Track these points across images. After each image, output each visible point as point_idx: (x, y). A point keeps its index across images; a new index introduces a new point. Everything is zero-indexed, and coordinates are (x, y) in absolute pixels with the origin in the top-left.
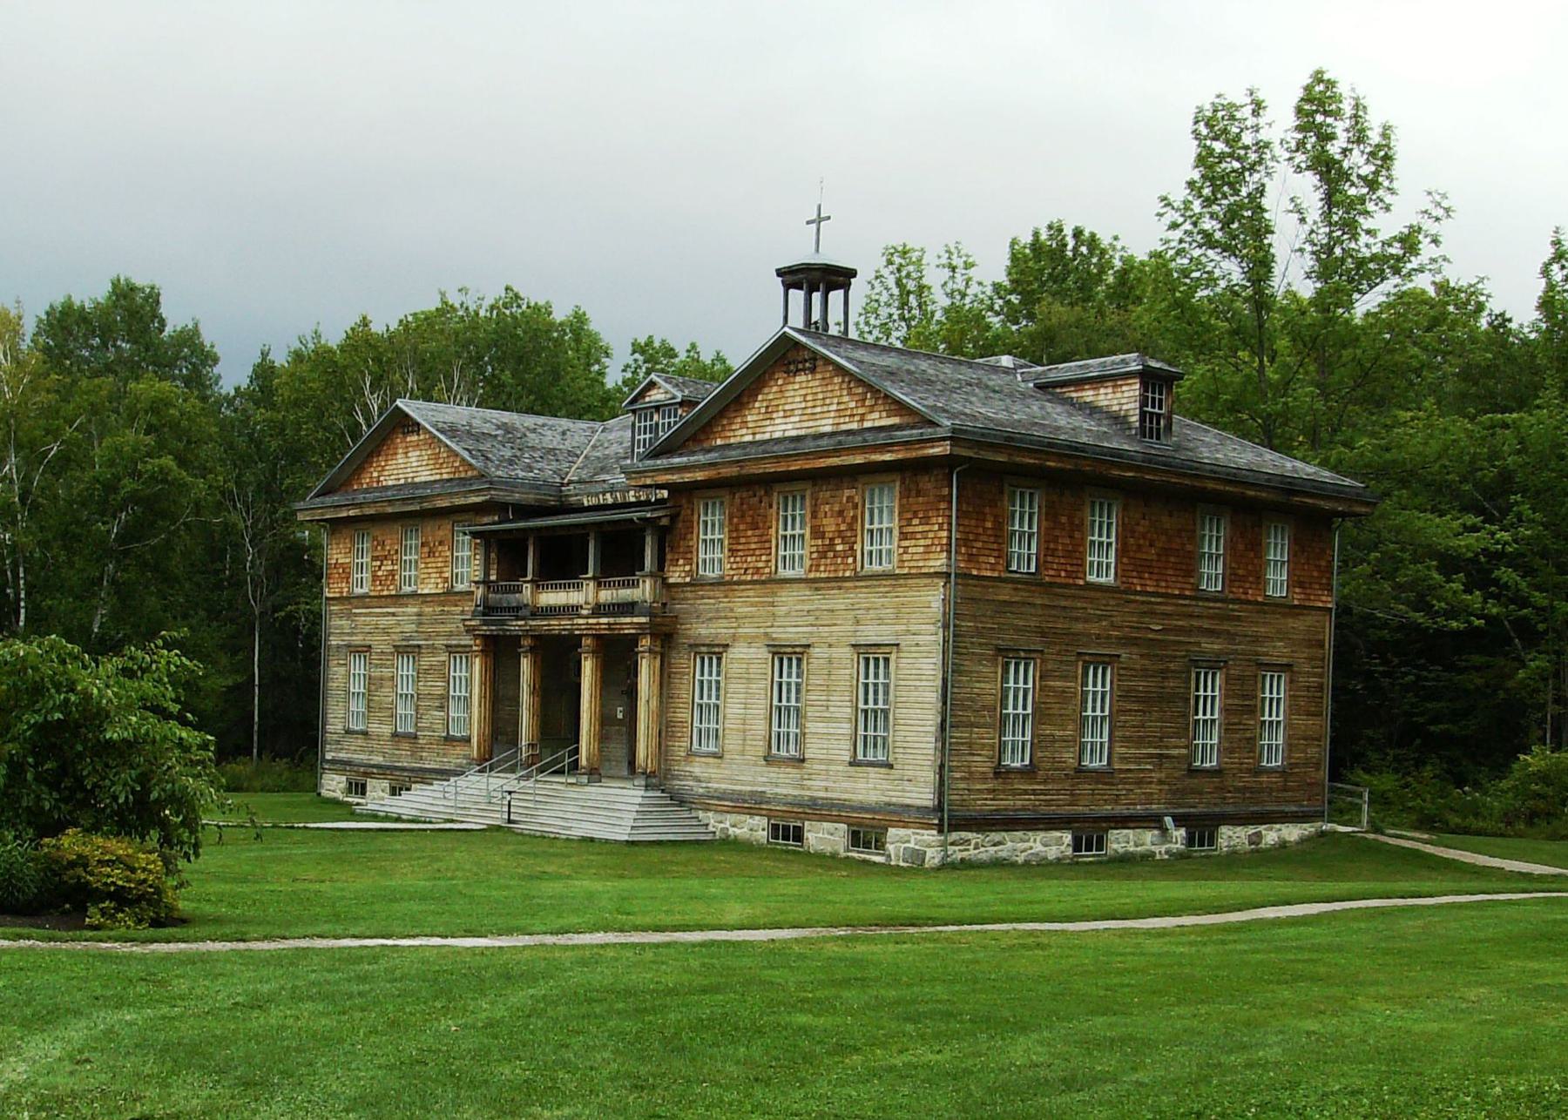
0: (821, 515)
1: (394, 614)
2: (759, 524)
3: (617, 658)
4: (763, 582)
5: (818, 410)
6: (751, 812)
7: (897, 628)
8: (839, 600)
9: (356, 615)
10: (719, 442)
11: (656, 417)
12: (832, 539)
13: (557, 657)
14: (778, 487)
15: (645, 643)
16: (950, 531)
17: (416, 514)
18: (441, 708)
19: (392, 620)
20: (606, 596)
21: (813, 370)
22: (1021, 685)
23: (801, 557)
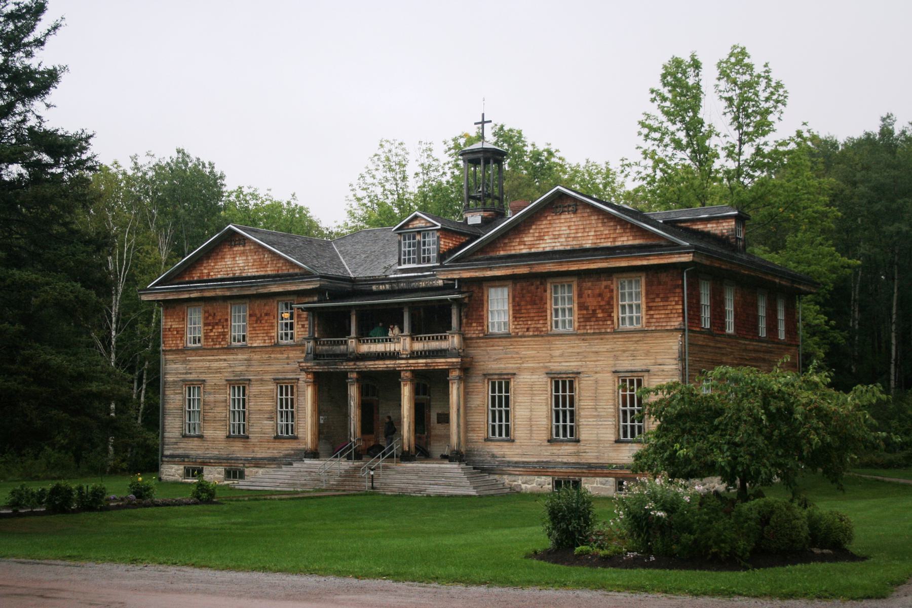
0: (585, 295)
1: (225, 360)
3: (430, 384)
4: (542, 336)
5: (580, 235)
6: (539, 473)
7: (647, 361)
8: (602, 346)
9: (190, 361)
10: (502, 253)
11: (418, 238)
12: (594, 311)
13: (378, 387)
14: (550, 281)
15: (455, 374)
16: (683, 305)
18: (271, 419)
20: (418, 346)
22: (284, 397)
23: (570, 321)
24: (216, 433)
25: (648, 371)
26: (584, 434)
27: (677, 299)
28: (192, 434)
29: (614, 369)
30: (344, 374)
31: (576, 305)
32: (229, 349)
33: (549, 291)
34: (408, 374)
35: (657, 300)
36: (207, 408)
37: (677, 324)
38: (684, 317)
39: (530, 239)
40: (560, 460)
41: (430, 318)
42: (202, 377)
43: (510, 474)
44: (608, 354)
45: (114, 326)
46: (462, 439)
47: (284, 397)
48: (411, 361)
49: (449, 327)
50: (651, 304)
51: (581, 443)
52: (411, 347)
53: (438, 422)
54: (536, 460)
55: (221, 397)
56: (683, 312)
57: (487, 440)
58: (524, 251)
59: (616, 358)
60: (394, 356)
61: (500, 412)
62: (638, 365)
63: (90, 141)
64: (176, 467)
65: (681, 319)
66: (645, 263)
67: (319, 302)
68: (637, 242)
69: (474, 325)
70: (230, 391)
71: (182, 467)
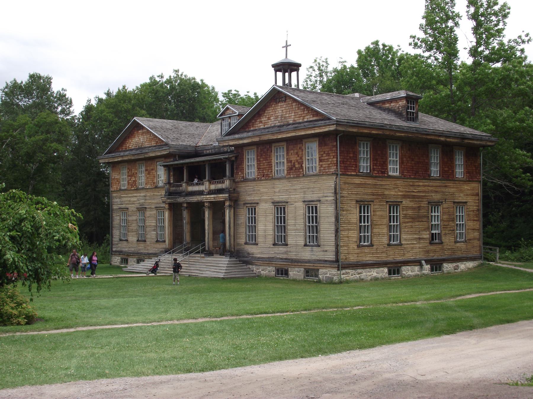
0: (290, 154)
1: (136, 196)
3: (217, 208)
5: (287, 115)
6: (269, 265)
9: (122, 197)
14: (274, 145)
15: (227, 204)
20: (213, 187)
21: (285, 101)
24: (133, 238)
25: (320, 201)
27: (333, 154)
29: (303, 200)
30: (181, 204)
31: (286, 160)
32: (137, 189)
33: (273, 151)
34: (185, 205)
35: (324, 155)
36: (129, 224)
37: (333, 170)
38: (337, 166)
39: (265, 119)
40: (278, 256)
41: (217, 170)
42: (128, 206)
43: (256, 265)
44: (301, 191)
46: (232, 242)
47: (311, 215)
48: (208, 196)
49: (225, 175)
51: (289, 246)
52: (209, 187)
54: (267, 256)
55: (134, 218)
56: (337, 163)
57: (246, 243)
58: (262, 127)
59: (305, 193)
60: (201, 193)
62: (315, 197)
64: (117, 258)
65: (335, 167)
66: (313, 132)
67: (174, 161)
68: (315, 118)
69: (240, 173)
70: (138, 214)
71: (120, 258)
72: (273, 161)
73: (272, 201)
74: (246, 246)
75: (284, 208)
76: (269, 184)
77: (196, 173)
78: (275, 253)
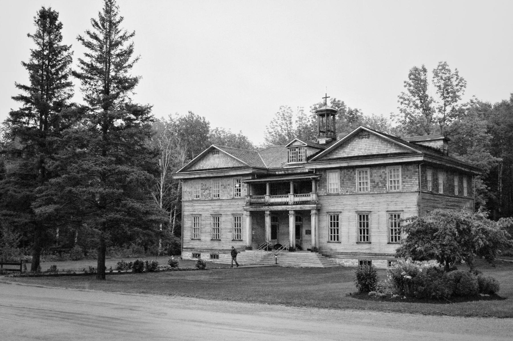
2: (351, 179)
3: (302, 217)
12: (378, 183)
13: (280, 218)
14: (357, 169)
17: (219, 175)
19: (209, 207)
20: (297, 199)
21: (368, 138)
25: (403, 211)
26: (373, 239)
28: (196, 238)
41: (303, 186)
42: (200, 213)
45: (162, 190)
50: (404, 180)
51: (372, 244)
53: (306, 234)
54: (351, 251)
59: (388, 205)
60: (286, 204)
61: (334, 230)
62: (398, 208)
63: (151, 108)
64: (188, 253)
72: (356, 181)
73: (355, 211)
74: (329, 244)
75: (367, 216)
76: (153, 274)
77: (280, 188)
78: (358, 249)
